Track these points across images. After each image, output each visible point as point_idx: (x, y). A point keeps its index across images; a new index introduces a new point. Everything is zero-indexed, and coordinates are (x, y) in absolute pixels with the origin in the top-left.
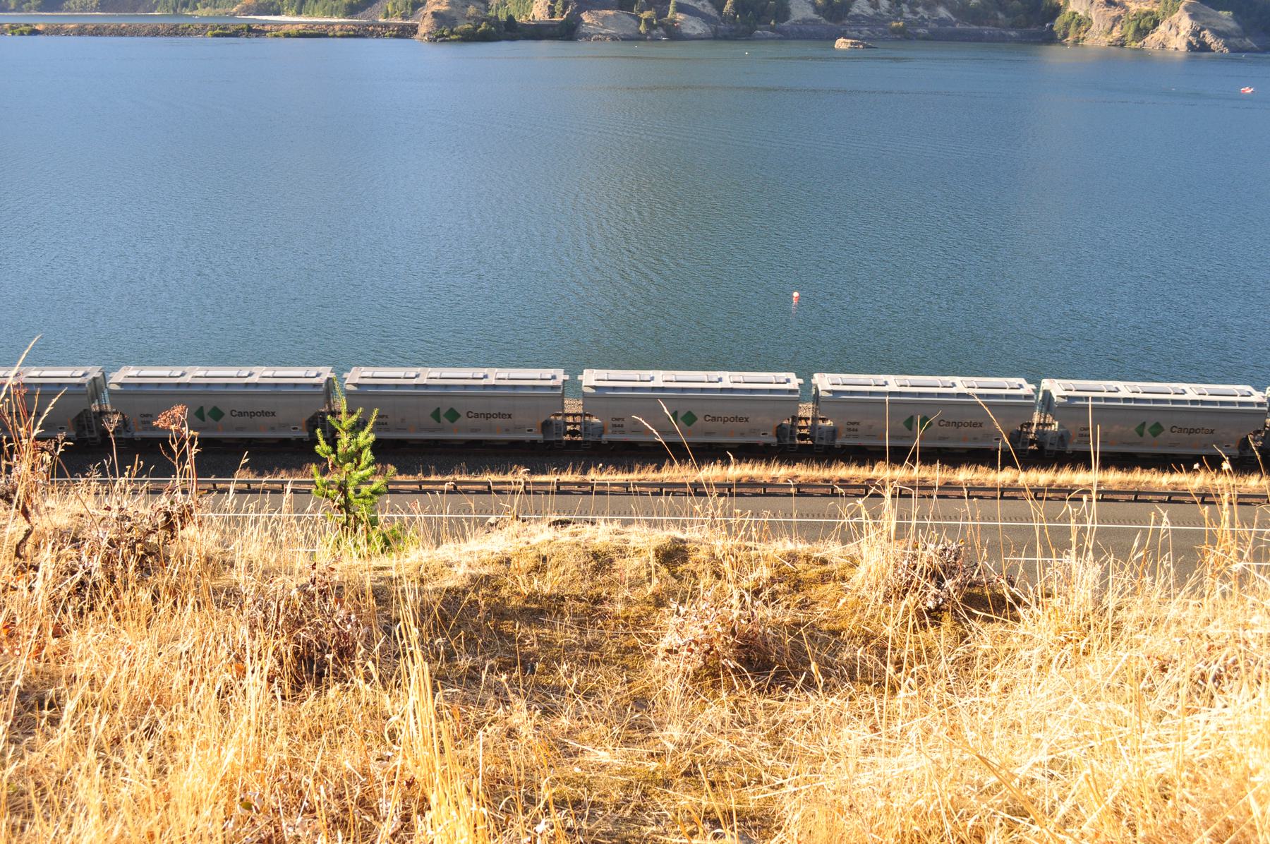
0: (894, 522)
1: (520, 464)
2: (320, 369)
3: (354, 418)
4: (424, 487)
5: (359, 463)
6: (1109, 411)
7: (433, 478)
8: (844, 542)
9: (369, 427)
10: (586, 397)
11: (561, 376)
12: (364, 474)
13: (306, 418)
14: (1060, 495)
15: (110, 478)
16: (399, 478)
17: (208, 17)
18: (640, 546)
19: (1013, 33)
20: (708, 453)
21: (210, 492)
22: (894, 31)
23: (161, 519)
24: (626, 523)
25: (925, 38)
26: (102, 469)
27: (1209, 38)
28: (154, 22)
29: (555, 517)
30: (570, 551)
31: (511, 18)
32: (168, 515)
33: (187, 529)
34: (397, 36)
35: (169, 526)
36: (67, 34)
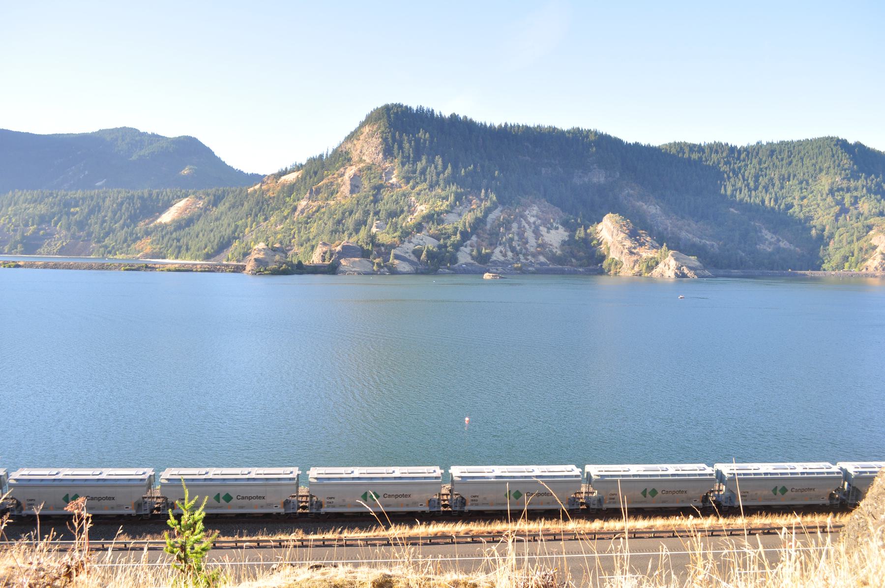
0: (514, 557)
1: (299, 528)
2: (145, 470)
3: (193, 502)
4: (239, 544)
5: (194, 531)
6: (629, 482)
7: (244, 538)
8: (487, 573)
9: (202, 507)
10: (311, 484)
11: (296, 471)
12: (199, 538)
13: (135, 500)
14: (609, 536)
15: (35, 542)
16: (222, 539)
17: (123, 259)
18: (363, 580)
19: (581, 270)
20: (408, 518)
21: (98, 550)
22: (516, 269)
23: (64, 570)
24: (356, 565)
25: (533, 273)
26: (30, 538)
27: (686, 271)
28: (89, 262)
29: (313, 563)
30: (320, 585)
31: (300, 263)
32: (69, 567)
33: (80, 576)
34: (234, 272)
35: (69, 575)
36: (37, 267)
